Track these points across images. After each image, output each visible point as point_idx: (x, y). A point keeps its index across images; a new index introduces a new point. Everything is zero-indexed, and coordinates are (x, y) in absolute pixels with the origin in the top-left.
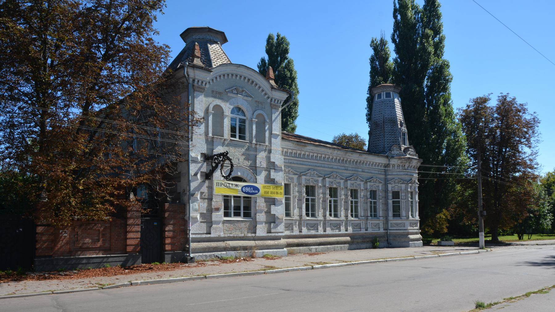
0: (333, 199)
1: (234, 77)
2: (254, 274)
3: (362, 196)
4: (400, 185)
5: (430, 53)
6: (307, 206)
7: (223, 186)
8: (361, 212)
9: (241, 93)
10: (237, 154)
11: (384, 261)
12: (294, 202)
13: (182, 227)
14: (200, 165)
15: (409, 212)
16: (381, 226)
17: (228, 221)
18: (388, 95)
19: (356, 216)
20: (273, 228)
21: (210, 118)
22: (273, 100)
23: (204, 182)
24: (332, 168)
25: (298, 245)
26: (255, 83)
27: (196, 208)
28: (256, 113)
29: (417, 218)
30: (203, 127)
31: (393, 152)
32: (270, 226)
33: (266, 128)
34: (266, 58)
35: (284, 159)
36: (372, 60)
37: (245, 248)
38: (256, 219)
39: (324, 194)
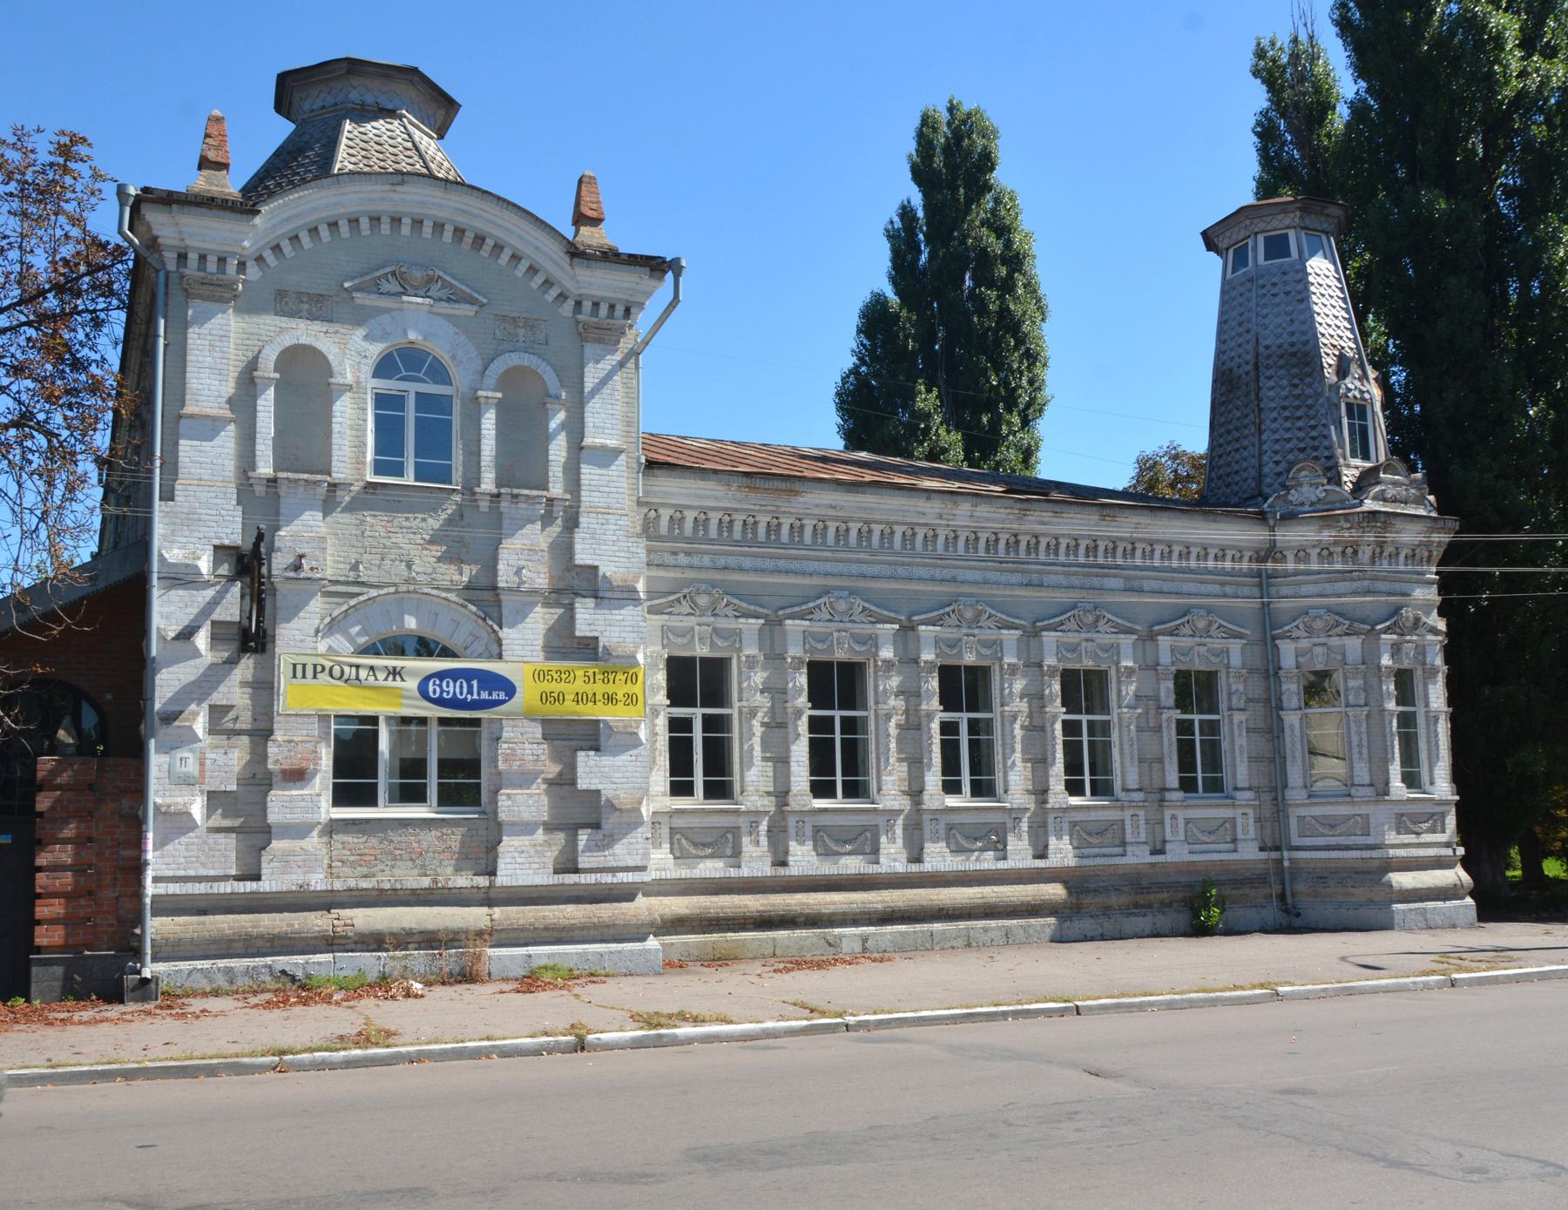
0: (963, 718)
1: (385, 228)
2: (211, 1071)
3: (1128, 699)
4: (1335, 641)
5: (1498, 41)
6: (1072, 751)
7: (324, 677)
8: (1125, 770)
9: (424, 287)
10: (400, 539)
11: (1062, 1013)
12: (746, 735)
13: (126, 853)
14: (209, 593)
15: (1386, 762)
16: (1248, 828)
17: (354, 822)
18: (1277, 247)
19: (1101, 789)
20: (588, 849)
21: (266, 404)
22: (587, 305)
23: (232, 662)
24: (954, 580)
25: (765, 922)
26: (490, 242)
27: (183, 776)
28: (498, 367)
29: (1442, 787)
30: (227, 441)
31: (1294, 496)
32: (572, 842)
33: (553, 425)
34: (917, 199)
35: (649, 551)
36: (1266, 133)
37: (430, 940)
38: (495, 813)
39: (911, 694)
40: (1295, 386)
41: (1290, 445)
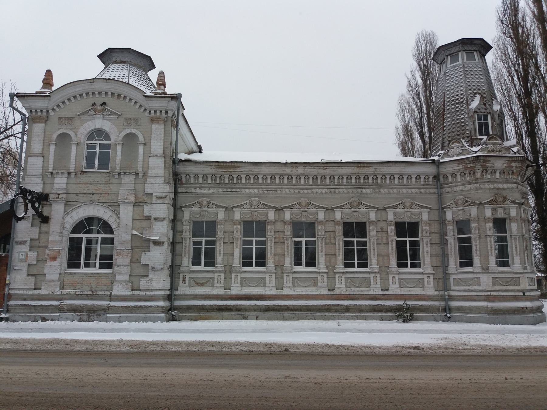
22: (152, 111)
41: (455, 134)
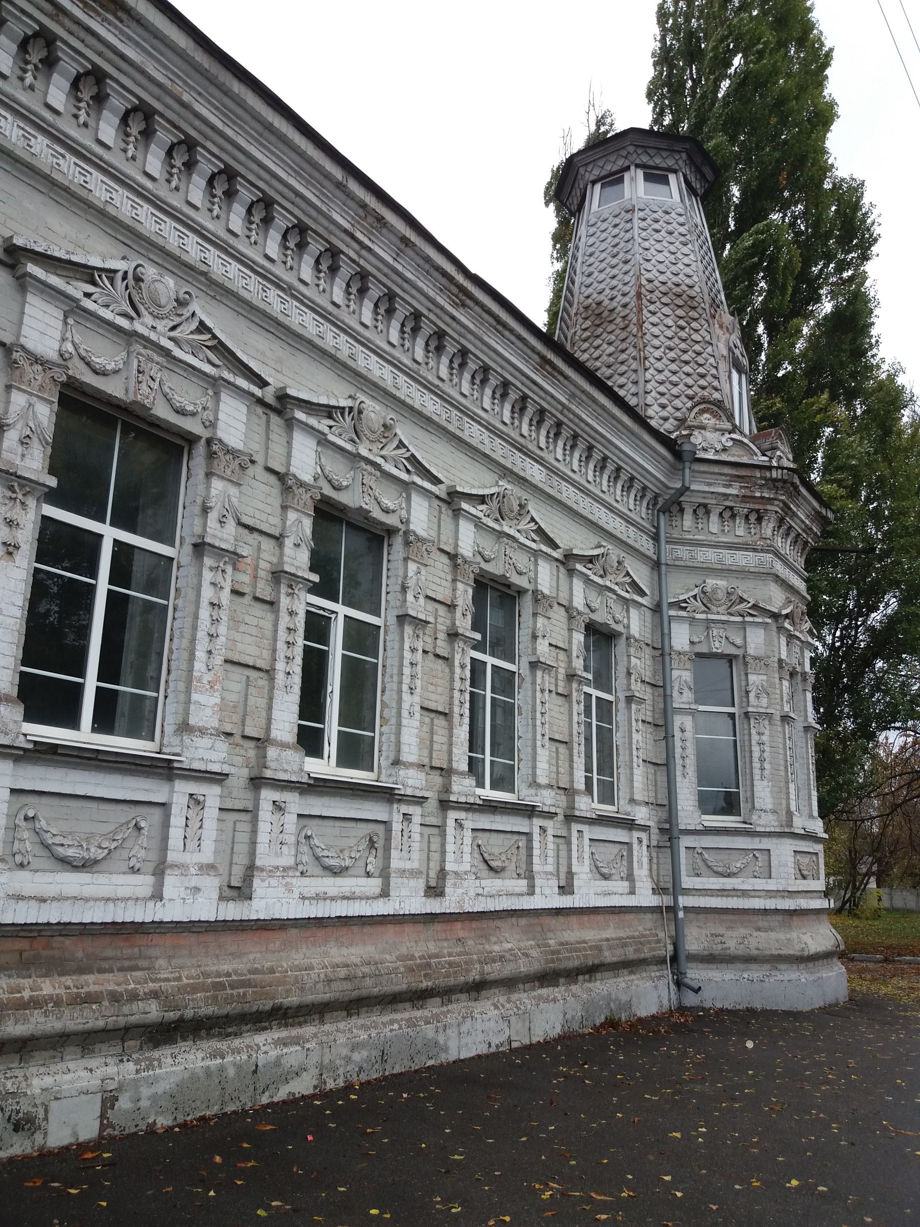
40: (682, 328)
